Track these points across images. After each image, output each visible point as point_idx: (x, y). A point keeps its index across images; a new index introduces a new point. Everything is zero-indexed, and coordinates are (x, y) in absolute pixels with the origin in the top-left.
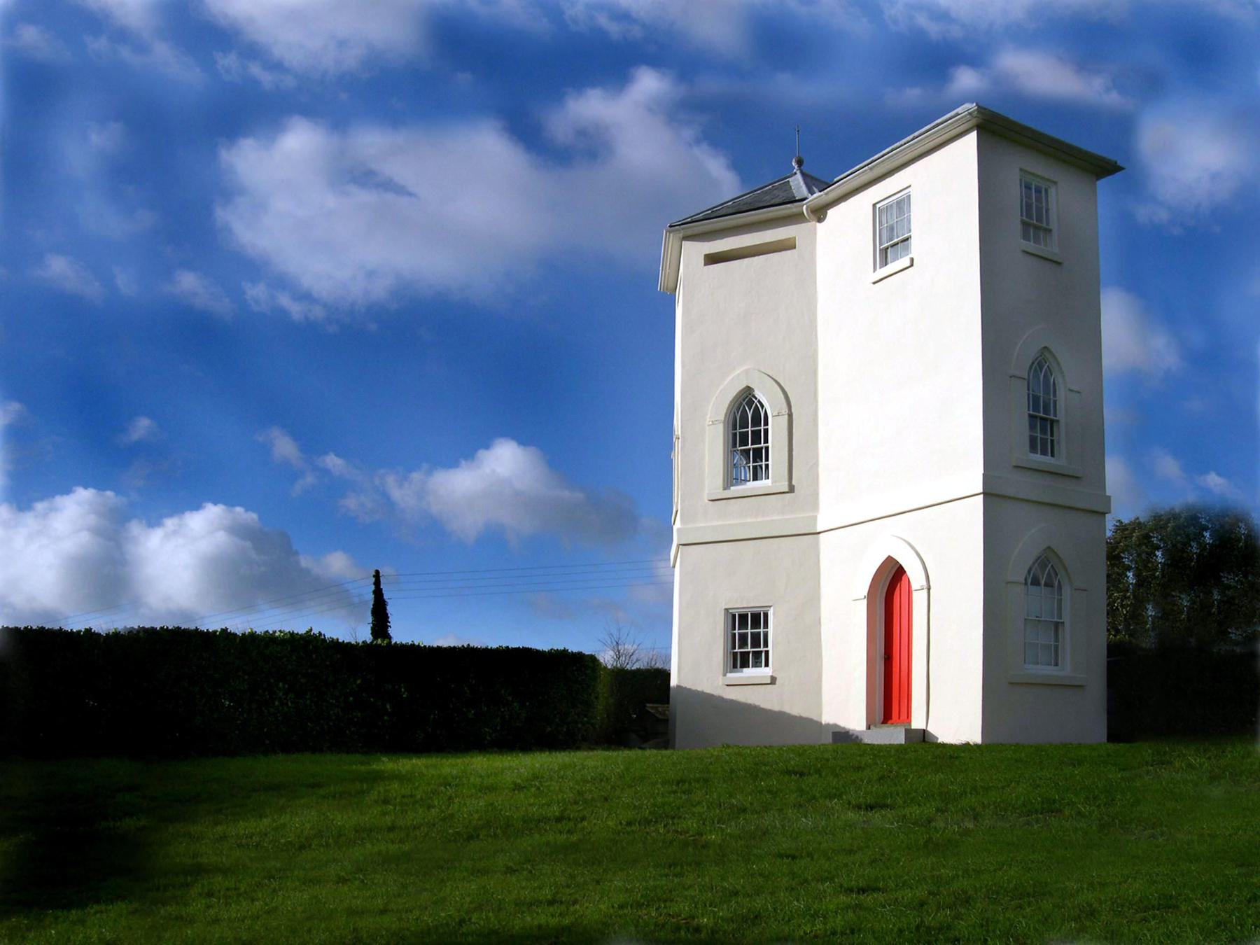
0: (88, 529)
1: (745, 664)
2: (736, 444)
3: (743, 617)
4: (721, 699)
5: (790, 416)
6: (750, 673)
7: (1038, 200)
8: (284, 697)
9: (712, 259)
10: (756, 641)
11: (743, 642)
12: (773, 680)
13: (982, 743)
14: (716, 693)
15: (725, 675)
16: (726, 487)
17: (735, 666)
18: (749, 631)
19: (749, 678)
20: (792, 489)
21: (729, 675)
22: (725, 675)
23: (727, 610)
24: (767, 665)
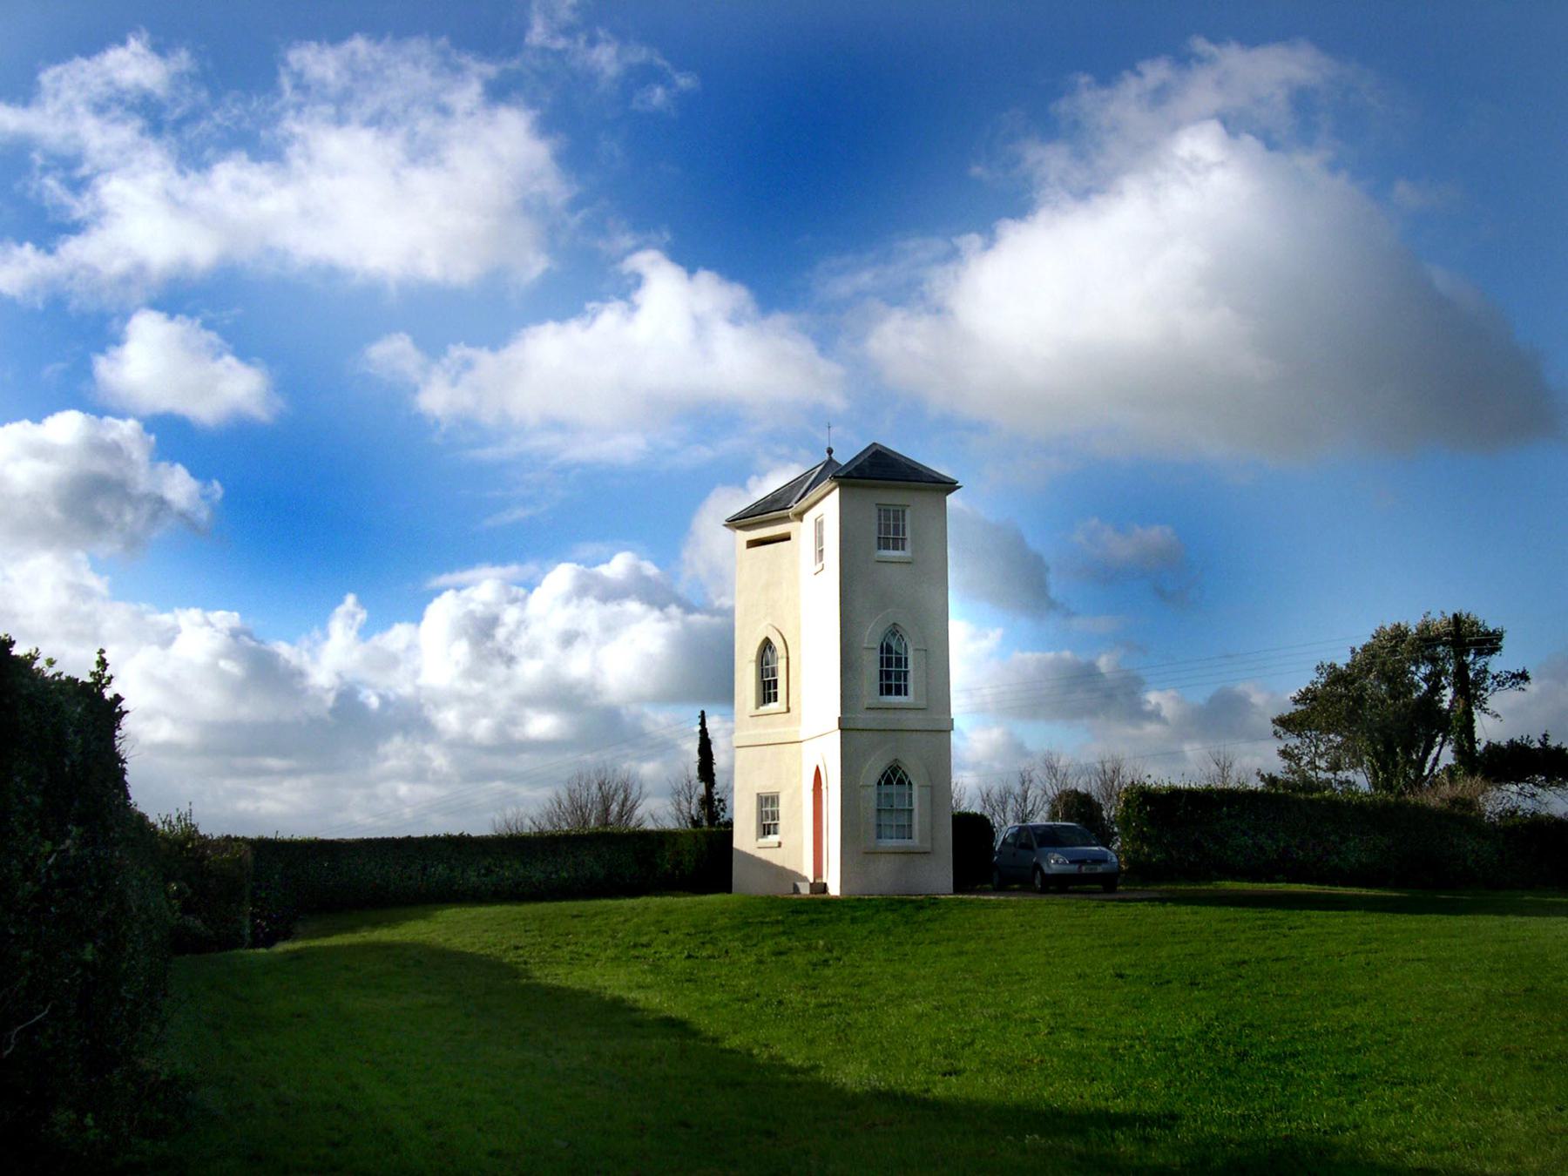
0: (160, 459)
1: (889, 693)
2: (762, 676)
3: (767, 799)
4: (752, 857)
5: (788, 658)
6: (894, 699)
7: (896, 519)
8: (501, 872)
9: (753, 544)
10: (888, 675)
11: (889, 664)
12: (780, 845)
13: (841, 894)
14: (752, 853)
15: (757, 840)
16: (757, 708)
17: (764, 834)
18: (894, 656)
19: (770, 842)
20: (788, 710)
21: (760, 840)
22: (757, 840)
23: (758, 794)
24: (906, 694)
